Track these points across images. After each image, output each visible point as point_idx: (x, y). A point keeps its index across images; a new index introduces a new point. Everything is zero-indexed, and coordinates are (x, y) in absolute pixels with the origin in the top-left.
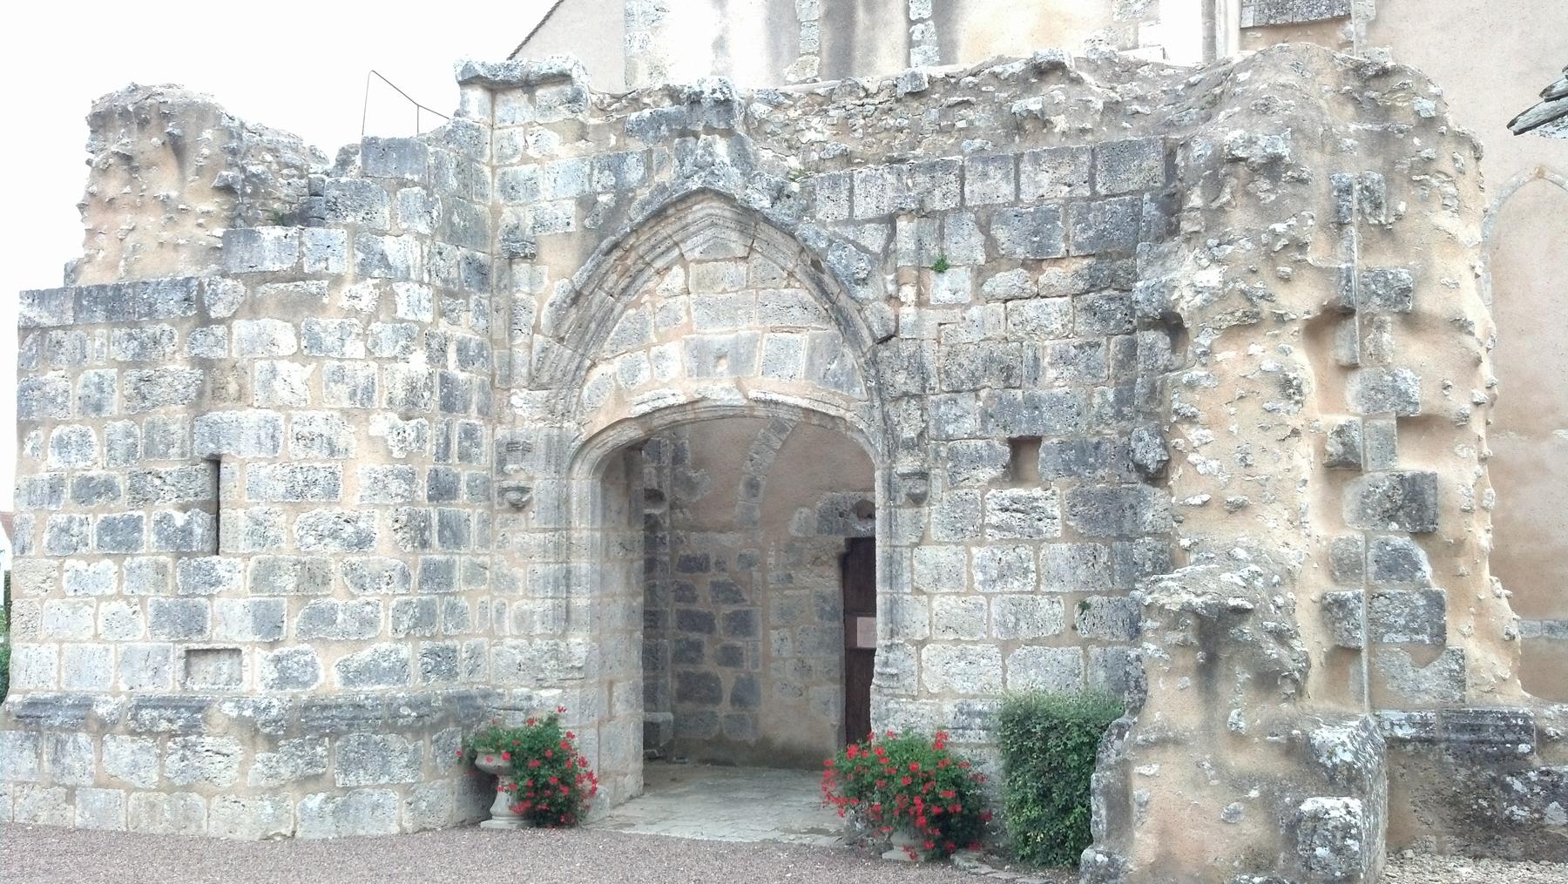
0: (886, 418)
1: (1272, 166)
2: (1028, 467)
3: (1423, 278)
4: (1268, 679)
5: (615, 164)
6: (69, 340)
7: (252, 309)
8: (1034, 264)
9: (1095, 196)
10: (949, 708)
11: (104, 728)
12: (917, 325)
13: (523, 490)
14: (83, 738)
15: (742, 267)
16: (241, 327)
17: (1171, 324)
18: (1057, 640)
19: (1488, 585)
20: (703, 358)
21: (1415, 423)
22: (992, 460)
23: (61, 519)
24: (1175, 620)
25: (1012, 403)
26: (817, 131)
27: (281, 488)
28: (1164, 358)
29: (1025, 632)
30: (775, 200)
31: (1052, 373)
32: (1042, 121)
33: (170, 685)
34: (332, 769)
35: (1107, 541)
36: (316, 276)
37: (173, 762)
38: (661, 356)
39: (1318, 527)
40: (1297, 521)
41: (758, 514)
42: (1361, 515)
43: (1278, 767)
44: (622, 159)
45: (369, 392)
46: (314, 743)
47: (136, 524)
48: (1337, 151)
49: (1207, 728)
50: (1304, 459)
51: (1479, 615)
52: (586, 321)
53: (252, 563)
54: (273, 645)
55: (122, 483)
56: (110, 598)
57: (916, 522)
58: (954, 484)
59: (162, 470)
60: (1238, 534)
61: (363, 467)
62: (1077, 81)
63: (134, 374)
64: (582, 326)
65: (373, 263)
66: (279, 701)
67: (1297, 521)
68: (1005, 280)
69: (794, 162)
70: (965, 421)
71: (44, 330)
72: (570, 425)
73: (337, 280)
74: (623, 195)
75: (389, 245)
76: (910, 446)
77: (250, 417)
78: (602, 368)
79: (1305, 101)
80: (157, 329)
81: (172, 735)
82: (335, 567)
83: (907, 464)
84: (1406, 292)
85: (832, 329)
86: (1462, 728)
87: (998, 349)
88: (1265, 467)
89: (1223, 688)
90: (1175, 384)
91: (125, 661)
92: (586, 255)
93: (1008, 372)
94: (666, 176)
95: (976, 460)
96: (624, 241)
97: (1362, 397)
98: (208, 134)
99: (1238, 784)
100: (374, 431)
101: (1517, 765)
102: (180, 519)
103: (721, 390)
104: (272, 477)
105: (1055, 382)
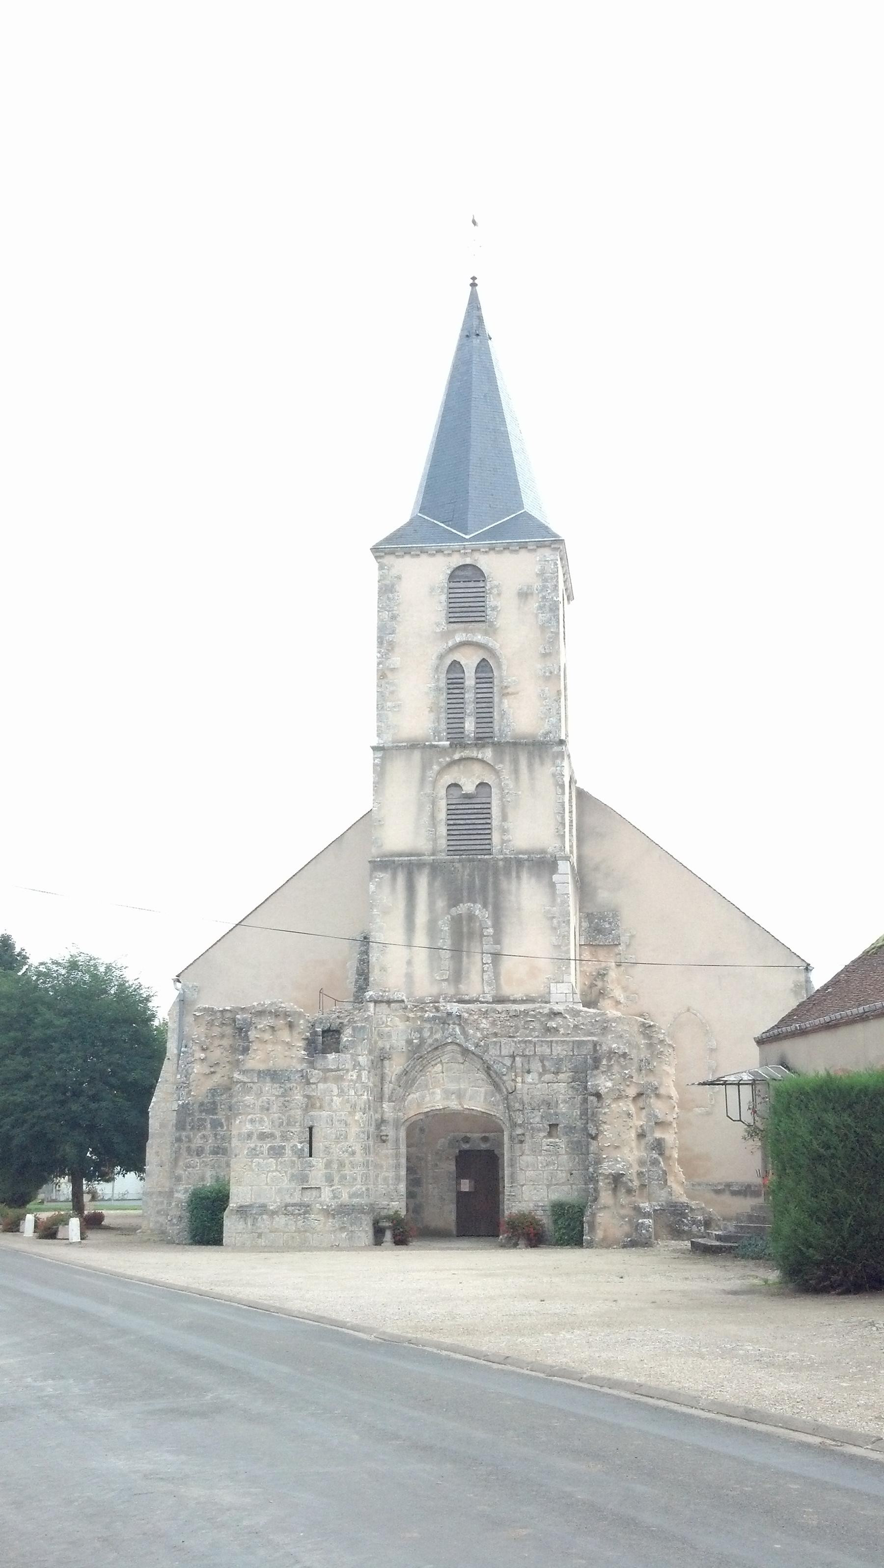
0: (510, 1116)
1: (624, 1055)
2: (554, 1133)
3: (661, 1084)
4: (629, 1191)
5: (420, 1030)
6: (255, 1087)
7: (325, 1080)
8: (556, 1073)
9: (574, 1055)
10: (531, 1205)
11: (274, 1213)
12: (522, 1089)
13: (387, 1136)
14: (265, 1217)
15: (462, 1066)
16: (321, 1086)
17: (598, 1095)
18: (563, 1184)
19: (677, 1168)
20: (447, 1094)
21: (659, 1124)
22: (544, 1131)
23: (252, 1145)
24: (607, 1177)
25: (550, 1114)
26: (484, 1024)
27: (334, 1136)
28: (595, 1104)
29: (554, 1182)
30: (476, 1047)
31: (562, 1105)
32: (556, 1030)
33: (296, 1199)
34: (348, 1225)
35: (578, 1155)
36: (342, 1070)
37: (300, 1223)
38: (433, 1093)
39: (636, 1152)
40: (631, 1151)
41: (424, 1140)
42: (646, 1148)
43: (632, 1213)
44: (422, 1029)
45: (355, 1105)
46: (344, 1216)
47: (283, 1147)
48: (639, 1049)
49: (615, 1204)
50: (633, 1134)
51: (675, 1176)
52: (407, 1080)
53: (325, 1160)
54: (331, 1186)
55: (278, 1134)
56: (273, 1171)
57: (521, 1148)
58: (533, 1137)
59: (293, 1130)
60: (618, 1155)
61: (354, 1130)
62: (566, 1018)
63: (282, 1099)
64: (407, 1082)
65: (357, 1065)
66: (334, 1204)
67: (631, 1151)
68: (548, 1077)
69: (479, 1035)
70: (536, 1119)
71: (245, 1083)
72: (400, 1114)
73: (348, 1071)
74: (422, 1040)
75: (360, 1059)
76: (520, 1125)
77: (324, 1114)
78: (412, 1096)
79: (631, 1035)
80: (291, 1085)
81: (300, 1215)
82: (347, 1162)
83: (519, 1131)
84: (656, 1088)
85: (492, 1088)
86: (671, 1206)
87: (546, 1098)
88: (624, 1137)
89: (619, 1194)
90: (601, 1112)
91: (279, 1191)
92: (409, 1059)
93: (549, 1104)
94: (438, 1036)
95: (539, 1130)
96: (420, 1055)
97: (646, 1116)
98: (301, 1022)
99: (623, 1217)
100: (356, 1118)
101: (685, 1215)
102: (299, 1146)
103: (454, 1104)
104: (331, 1133)
105: (563, 1108)
